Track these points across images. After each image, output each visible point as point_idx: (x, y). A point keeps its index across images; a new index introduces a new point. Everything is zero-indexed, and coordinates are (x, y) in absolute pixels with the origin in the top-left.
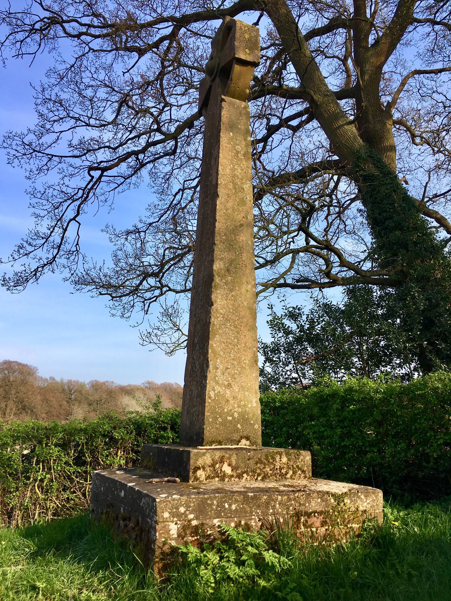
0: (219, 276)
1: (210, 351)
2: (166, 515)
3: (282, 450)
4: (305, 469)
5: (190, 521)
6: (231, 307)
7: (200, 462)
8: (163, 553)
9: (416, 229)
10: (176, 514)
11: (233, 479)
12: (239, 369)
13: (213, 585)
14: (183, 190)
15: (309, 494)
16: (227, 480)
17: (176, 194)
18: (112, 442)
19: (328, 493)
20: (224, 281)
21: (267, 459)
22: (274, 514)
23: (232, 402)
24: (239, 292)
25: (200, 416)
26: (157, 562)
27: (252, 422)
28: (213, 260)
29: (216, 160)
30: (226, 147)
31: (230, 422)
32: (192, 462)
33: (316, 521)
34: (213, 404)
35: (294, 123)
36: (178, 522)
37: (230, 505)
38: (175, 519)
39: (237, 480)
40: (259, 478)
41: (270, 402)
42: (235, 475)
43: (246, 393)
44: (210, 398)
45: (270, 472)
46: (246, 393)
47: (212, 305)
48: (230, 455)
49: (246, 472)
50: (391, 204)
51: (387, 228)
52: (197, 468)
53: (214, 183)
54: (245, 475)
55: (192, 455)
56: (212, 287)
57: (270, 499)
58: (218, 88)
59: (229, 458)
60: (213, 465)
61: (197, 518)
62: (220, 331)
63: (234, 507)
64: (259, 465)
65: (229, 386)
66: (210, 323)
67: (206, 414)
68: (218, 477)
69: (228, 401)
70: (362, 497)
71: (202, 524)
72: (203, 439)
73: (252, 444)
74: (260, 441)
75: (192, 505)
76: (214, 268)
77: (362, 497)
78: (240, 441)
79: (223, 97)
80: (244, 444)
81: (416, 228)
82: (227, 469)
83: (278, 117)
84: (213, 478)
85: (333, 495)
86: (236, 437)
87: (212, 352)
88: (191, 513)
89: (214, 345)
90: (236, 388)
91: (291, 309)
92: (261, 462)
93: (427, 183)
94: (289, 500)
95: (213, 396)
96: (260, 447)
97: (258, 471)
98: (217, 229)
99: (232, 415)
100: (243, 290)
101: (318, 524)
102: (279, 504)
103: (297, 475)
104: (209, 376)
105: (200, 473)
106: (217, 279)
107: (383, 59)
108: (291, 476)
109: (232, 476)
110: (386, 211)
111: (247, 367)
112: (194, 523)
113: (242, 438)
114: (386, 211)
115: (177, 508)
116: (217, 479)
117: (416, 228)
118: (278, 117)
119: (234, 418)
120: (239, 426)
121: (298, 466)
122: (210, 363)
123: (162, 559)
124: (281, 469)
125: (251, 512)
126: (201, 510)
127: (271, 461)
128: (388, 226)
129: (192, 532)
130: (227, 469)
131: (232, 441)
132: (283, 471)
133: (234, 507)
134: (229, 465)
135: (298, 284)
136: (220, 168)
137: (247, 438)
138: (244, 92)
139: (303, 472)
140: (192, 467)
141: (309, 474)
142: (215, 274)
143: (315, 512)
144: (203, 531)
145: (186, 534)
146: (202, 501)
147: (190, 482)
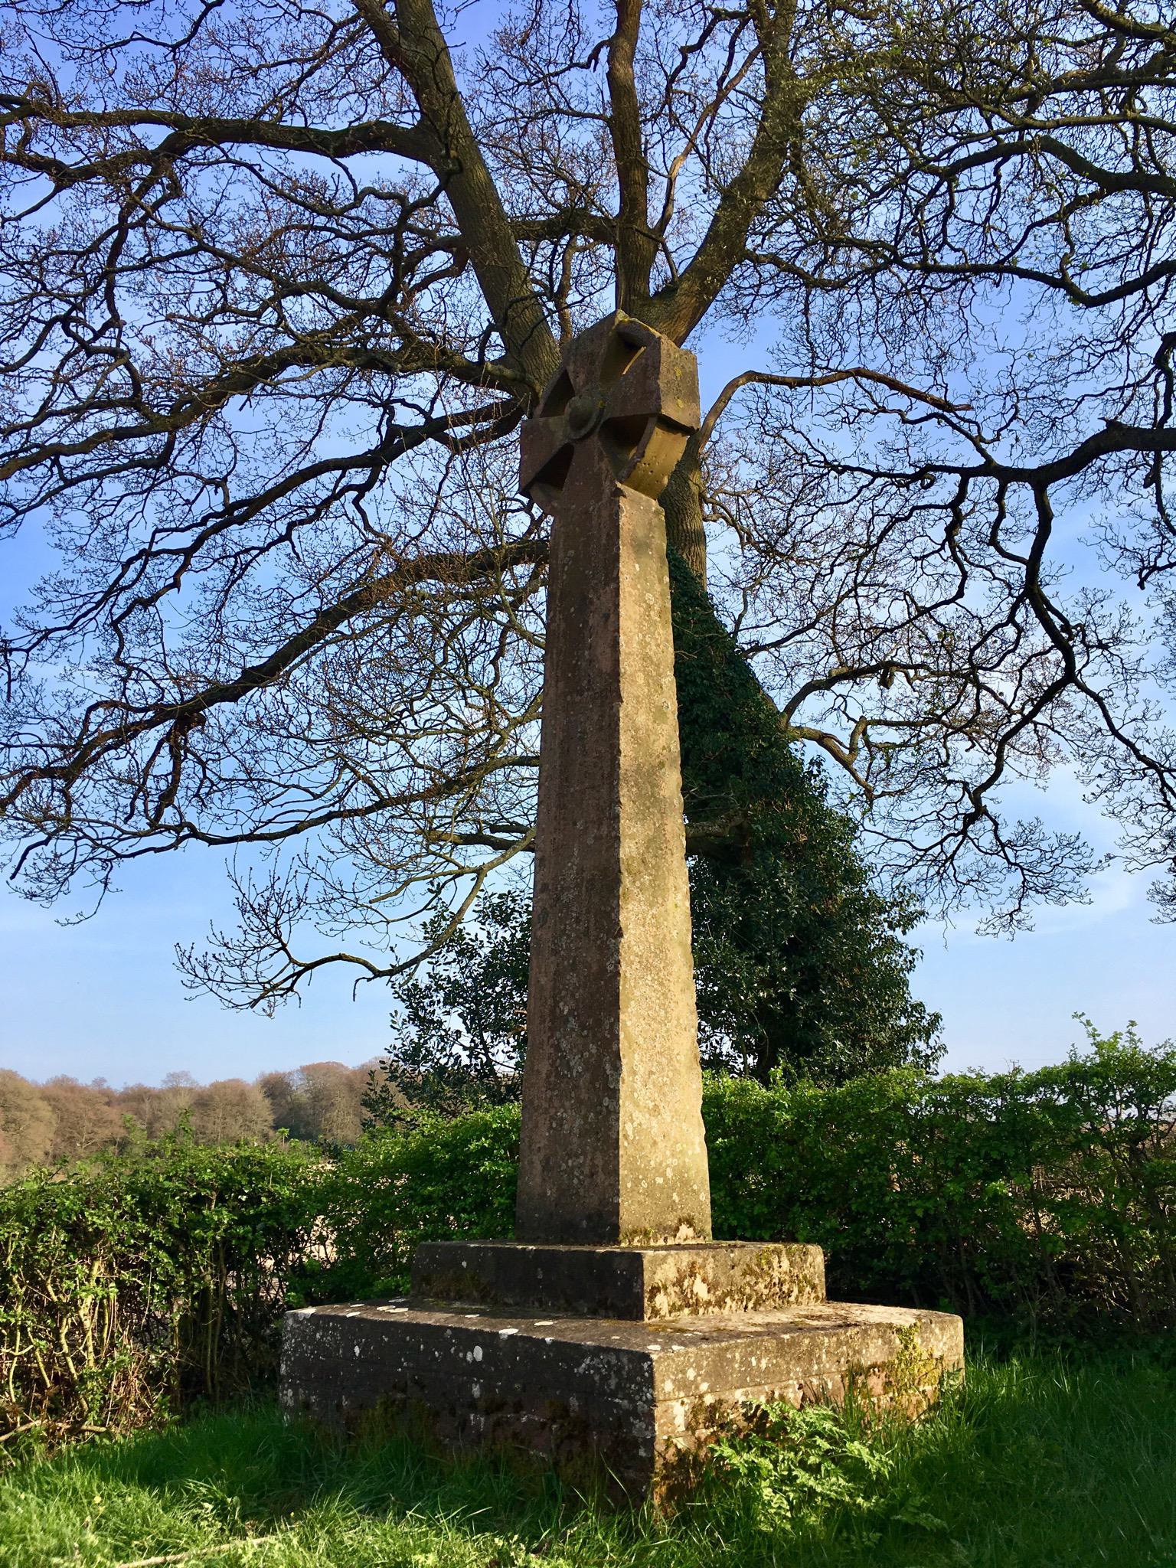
0: (629, 873)
1: (622, 1036)
2: (668, 1386)
3: (780, 1246)
4: (816, 1281)
5: (701, 1397)
6: (651, 940)
7: (659, 1278)
8: (665, 1465)
9: (756, 730)
10: (683, 1385)
11: (710, 1309)
12: (671, 1074)
13: (789, 1514)
14: (146, 555)
15: (865, 1331)
16: (701, 1311)
17: (131, 561)
18: (82, 1240)
19: (890, 1326)
20: (638, 884)
21: (759, 1265)
22: (819, 1374)
23: (661, 1145)
24: (662, 909)
25: (601, 1177)
26: (657, 1484)
27: (695, 1187)
28: (618, 838)
29: (607, 617)
30: (630, 594)
31: (662, 1188)
32: (646, 1276)
33: (876, 1383)
34: (631, 1151)
35: (461, 432)
36: (686, 1400)
37: (759, 1361)
38: (682, 1394)
39: (716, 1309)
40: (750, 1305)
41: (508, 1132)
42: (713, 1300)
43: (685, 1126)
44: (626, 1137)
45: (766, 1291)
46: (685, 1126)
47: (621, 936)
48: (705, 1259)
49: (730, 1293)
50: (703, 668)
51: (695, 721)
52: (655, 1290)
53: (606, 665)
54: (728, 1300)
55: (645, 1261)
56: (618, 897)
57: (814, 1345)
58: (601, 459)
59: (703, 1267)
60: (679, 1283)
61: (712, 1390)
62: (637, 993)
63: (764, 1364)
64: (748, 1278)
65: (656, 1111)
66: (618, 974)
67: (621, 1172)
68: (688, 1305)
69: (655, 1143)
70: (937, 1331)
71: (720, 1402)
72: (616, 1228)
73: (699, 1233)
74: (708, 1228)
75: (705, 1363)
76: (621, 855)
77: (937, 1331)
78: (677, 1230)
79: (619, 485)
80: (685, 1231)
81: (756, 728)
82: (701, 1290)
83: (422, 411)
84: (680, 1308)
85: (899, 1330)
86: (671, 1220)
87: (626, 1037)
88: (703, 1381)
89: (629, 1023)
90: (667, 1116)
91: (495, 900)
92: (752, 1272)
93: (741, 616)
94: (839, 1344)
95: (630, 1133)
96: (709, 1240)
97: (748, 1290)
98: (622, 772)
99: (663, 1175)
100: (670, 905)
101: (879, 1389)
102: (827, 1352)
103: (806, 1296)
104: (624, 1089)
105: (662, 1301)
106: (626, 880)
107: (683, 330)
108: (797, 1298)
109: (709, 1303)
110: (694, 683)
111: (683, 1070)
112: (709, 1400)
113: (680, 1222)
114: (694, 683)
115: (683, 1372)
116: (687, 1311)
117: (756, 728)
118: (422, 411)
119: (666, 1180)
120: (675, 1197)
121: (805, 1277)
122: (624, 1061)
123: (665, 1478)
124: (781, 1283)
125: (788, 1373)
126: (718, 1374)
127: (766, 1267)
128: (698, 716)
129: (706, 1420)
130: (701, 1290)
131: (665, 1229)
132: (785, 1288)
133: (764, 1364)
134: (704, 1280)
135: (498, 835)
136: (622, 639)
137: (690, 1222)
138: (659, 481)
139: (814, 1287)
140: (647, 1288)
141: (822, 1292)
142: (623, 868)
143: (873, 1366)
144: (722, 1416)
145: (698, 1423)
146: (719, 1355)
147: (646, 1320)
